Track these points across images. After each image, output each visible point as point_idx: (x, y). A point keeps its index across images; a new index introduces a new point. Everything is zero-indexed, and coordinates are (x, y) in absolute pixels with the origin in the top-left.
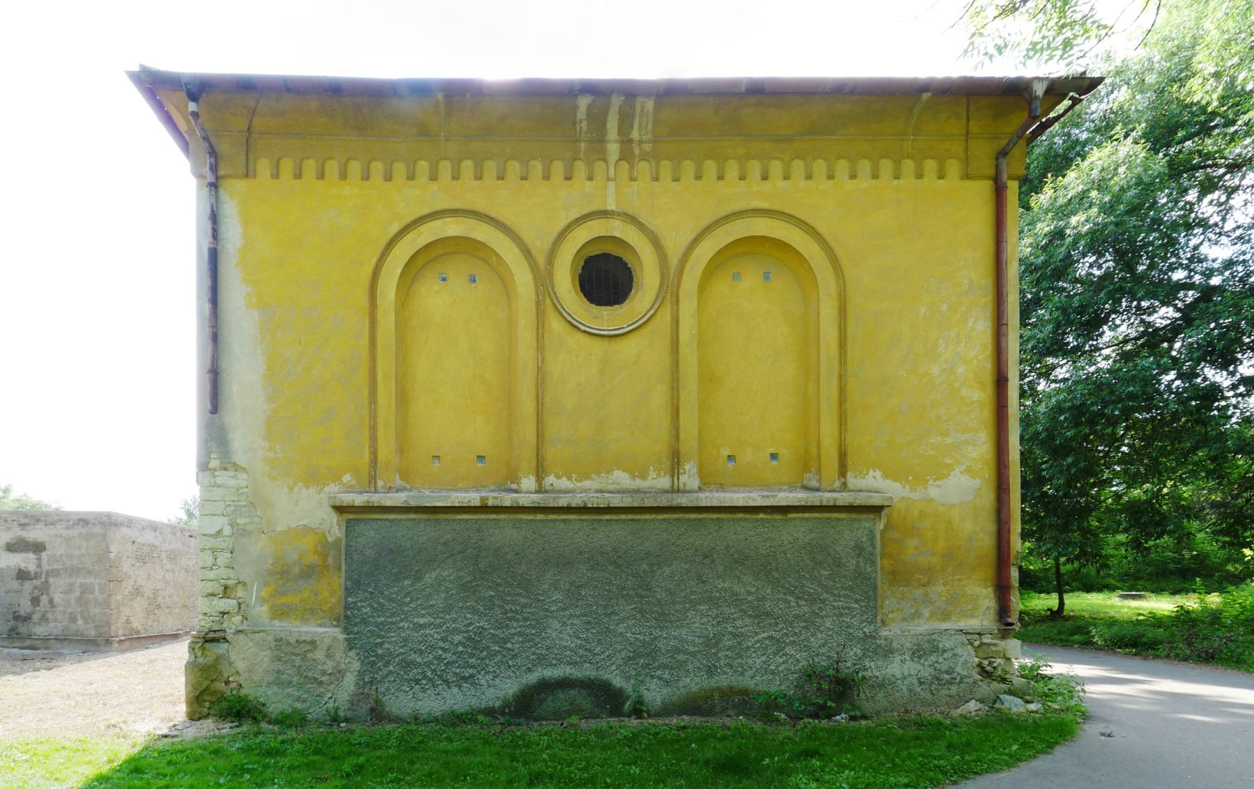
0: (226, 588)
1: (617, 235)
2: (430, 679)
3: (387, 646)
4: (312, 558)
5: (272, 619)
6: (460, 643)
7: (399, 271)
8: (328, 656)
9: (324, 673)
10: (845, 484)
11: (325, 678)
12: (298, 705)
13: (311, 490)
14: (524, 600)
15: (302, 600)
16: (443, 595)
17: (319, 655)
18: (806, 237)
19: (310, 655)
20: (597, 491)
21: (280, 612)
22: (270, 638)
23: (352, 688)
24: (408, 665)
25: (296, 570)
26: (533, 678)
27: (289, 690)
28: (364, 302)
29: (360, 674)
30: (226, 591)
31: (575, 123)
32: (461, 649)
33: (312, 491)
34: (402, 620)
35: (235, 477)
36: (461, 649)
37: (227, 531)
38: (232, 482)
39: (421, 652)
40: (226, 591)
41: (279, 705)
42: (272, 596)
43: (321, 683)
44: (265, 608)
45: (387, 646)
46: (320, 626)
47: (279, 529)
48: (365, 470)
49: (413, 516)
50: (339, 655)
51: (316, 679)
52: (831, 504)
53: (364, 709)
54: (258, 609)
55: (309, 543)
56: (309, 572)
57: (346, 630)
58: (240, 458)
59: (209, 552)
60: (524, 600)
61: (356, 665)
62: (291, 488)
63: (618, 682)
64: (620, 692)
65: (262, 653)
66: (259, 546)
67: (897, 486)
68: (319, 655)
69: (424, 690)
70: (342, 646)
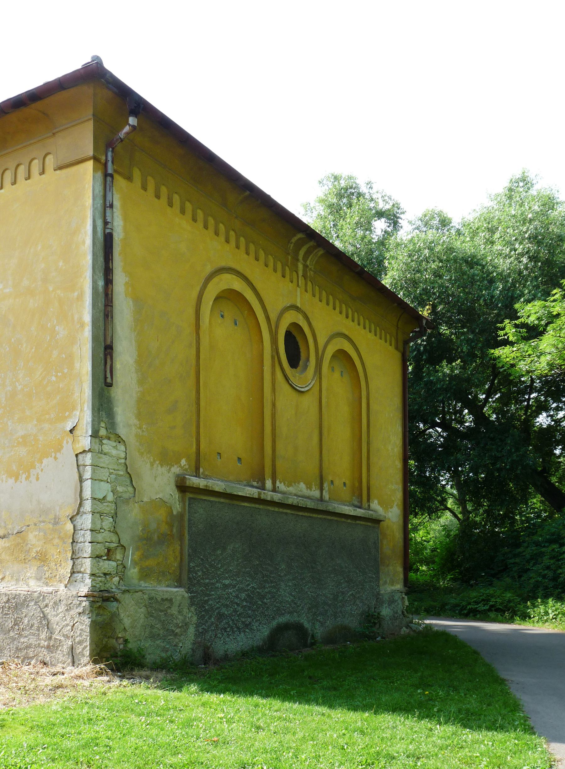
0: (109, 550)
1: (301, 324)
2: (232, 627)
3: (210, 602)
4: (164, 528)
5: (140, 580)
6: (245, 599)
7: (211, 303)
8: (179, 612)
9: (177, 626)
10: (369, 506)
11: (178, 631)
12: (163, 655)
13: (163, 468)
14: (270, 568)
15: (158, 564)
16: (236, 563)
17: (174, 610)
18: (358, 359)
19: (169, 611)
20: (295, 495)
21: (145, 574)
22: (146, 597)
23: (193, 638)
24: (221, 616)
25: (155, 537)
26: (274, 623)
27: (158, 642)
28: (371, 401)
29: (197, 626)
30: (109, 554)
31: (289, 242)
32: (245, 604)
33: (164, 469)
34: (217, 582)
35: (115, 447)
36: (245, 604)
37: (110, 497)
38: (114, 452)
39: (227, 606)
40: (109, 554)
41: (152, 656)
42: (141, 560)
43: (176, 635)
44: (136, 570)
45: (210, 602)
46: (168, 586)
47: (145, 499)
48: (193, 457)
49: (222, 500)
50: (185, 610)
51: (173, 631)
52: (191, 486)
53: (199, 654)
54: (132, 571)
55: (162, 514)
56: (164, 539)
57: (189, 591)
58: (122, 431)
59: (98, 515)
60: (270, 568)
61: (195, 619)
62: (152, 465)
63: (307, 625)
64: (307, 630)
65: (140, 610)
66: (133, 513)
67: (381, 509)
68: (174, 610)
69: (228, 636)
70: (187, 602)
